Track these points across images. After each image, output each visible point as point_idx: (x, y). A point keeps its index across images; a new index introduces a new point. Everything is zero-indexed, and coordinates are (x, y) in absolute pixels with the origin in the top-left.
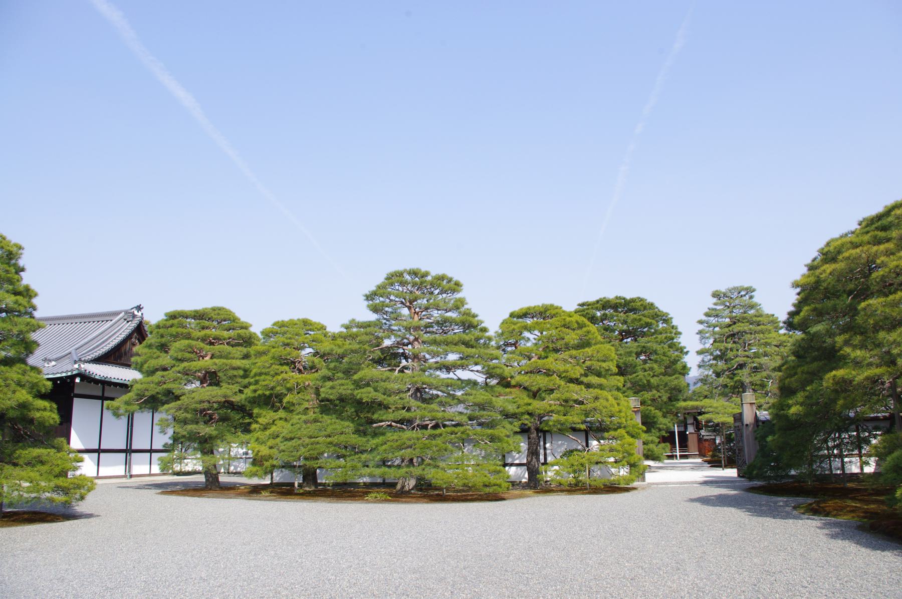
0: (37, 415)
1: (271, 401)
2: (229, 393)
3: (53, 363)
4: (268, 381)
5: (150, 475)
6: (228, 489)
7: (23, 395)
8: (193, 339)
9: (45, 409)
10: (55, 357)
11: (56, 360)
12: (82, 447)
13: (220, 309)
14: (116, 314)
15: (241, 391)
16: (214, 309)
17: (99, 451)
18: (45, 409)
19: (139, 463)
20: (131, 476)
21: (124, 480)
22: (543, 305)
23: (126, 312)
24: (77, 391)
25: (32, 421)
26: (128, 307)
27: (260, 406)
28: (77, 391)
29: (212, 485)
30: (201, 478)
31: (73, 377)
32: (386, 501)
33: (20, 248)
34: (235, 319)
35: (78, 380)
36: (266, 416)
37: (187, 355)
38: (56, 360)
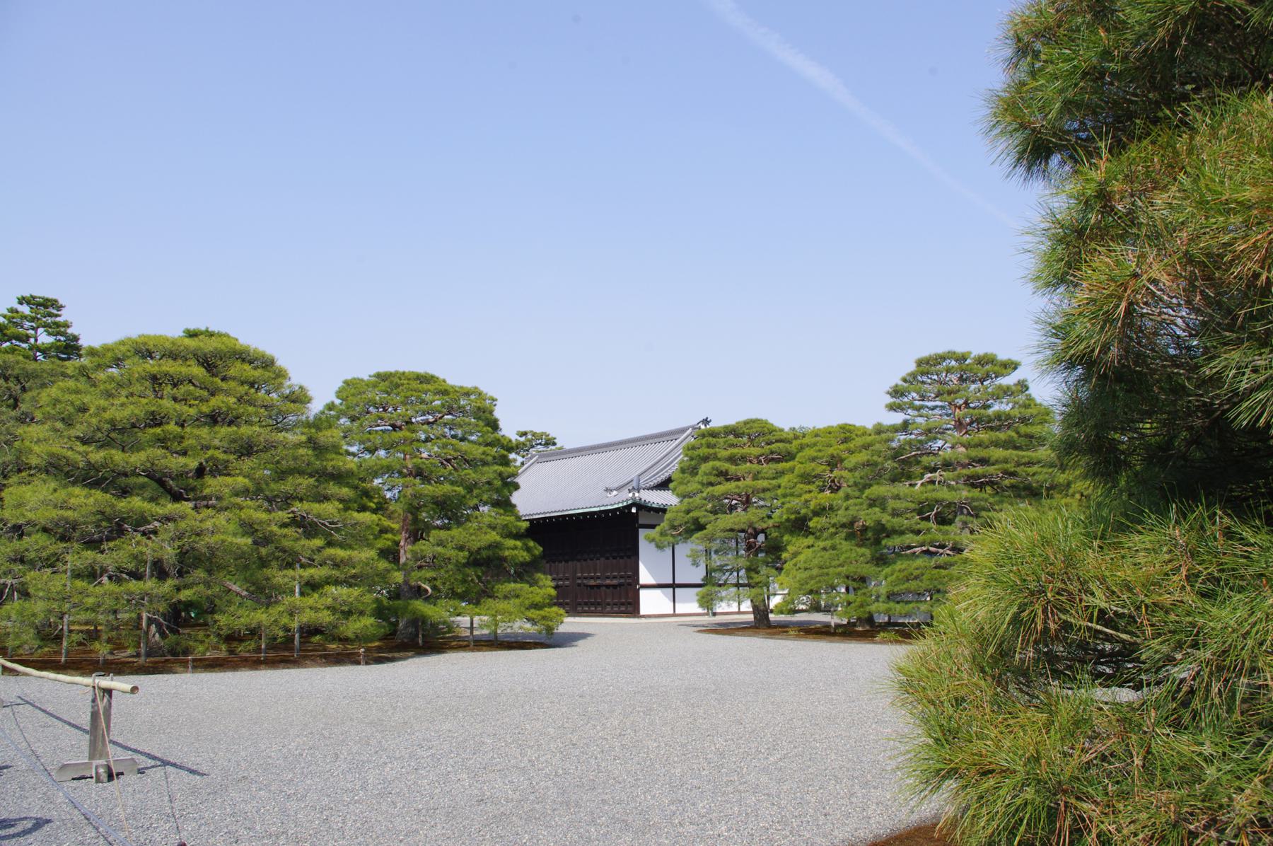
0: (507, 553)
1: (799, 525)
2: (754, 519)
3: (615, 493)
4: (795, 503)
5: (739, 613)
6: (780, 629)
7: (493, 536)
8: (719, 460)
9: (515, 548)
10: (616, 485)
11: (618, 489)
12: (653, 582)
13: (754, 421)
14: (683, 431)
15: (769, 517)
16: (746, 423)
17: (674, 586)
18: (515, 548)
19: (684, 601)
20: (715, 614)
21: (706, 618)
22: (801, 428)
23: (694, 428)
24: (641, 522)
25: (504, 559)
26: (694, 422)
27: (792, 533)
28: (641, 522)
29: (762, 623)
30: (751, 617)
31: (629, 507)
32: (897, 642)
33: (494, 400)
34: (772, 430)
35: (634, 510)
36: (795, 544)
37: (713, 479)
38: (618, 489)
